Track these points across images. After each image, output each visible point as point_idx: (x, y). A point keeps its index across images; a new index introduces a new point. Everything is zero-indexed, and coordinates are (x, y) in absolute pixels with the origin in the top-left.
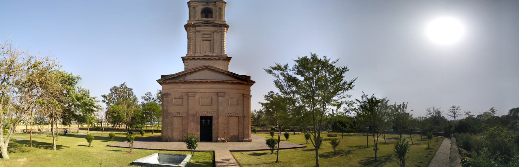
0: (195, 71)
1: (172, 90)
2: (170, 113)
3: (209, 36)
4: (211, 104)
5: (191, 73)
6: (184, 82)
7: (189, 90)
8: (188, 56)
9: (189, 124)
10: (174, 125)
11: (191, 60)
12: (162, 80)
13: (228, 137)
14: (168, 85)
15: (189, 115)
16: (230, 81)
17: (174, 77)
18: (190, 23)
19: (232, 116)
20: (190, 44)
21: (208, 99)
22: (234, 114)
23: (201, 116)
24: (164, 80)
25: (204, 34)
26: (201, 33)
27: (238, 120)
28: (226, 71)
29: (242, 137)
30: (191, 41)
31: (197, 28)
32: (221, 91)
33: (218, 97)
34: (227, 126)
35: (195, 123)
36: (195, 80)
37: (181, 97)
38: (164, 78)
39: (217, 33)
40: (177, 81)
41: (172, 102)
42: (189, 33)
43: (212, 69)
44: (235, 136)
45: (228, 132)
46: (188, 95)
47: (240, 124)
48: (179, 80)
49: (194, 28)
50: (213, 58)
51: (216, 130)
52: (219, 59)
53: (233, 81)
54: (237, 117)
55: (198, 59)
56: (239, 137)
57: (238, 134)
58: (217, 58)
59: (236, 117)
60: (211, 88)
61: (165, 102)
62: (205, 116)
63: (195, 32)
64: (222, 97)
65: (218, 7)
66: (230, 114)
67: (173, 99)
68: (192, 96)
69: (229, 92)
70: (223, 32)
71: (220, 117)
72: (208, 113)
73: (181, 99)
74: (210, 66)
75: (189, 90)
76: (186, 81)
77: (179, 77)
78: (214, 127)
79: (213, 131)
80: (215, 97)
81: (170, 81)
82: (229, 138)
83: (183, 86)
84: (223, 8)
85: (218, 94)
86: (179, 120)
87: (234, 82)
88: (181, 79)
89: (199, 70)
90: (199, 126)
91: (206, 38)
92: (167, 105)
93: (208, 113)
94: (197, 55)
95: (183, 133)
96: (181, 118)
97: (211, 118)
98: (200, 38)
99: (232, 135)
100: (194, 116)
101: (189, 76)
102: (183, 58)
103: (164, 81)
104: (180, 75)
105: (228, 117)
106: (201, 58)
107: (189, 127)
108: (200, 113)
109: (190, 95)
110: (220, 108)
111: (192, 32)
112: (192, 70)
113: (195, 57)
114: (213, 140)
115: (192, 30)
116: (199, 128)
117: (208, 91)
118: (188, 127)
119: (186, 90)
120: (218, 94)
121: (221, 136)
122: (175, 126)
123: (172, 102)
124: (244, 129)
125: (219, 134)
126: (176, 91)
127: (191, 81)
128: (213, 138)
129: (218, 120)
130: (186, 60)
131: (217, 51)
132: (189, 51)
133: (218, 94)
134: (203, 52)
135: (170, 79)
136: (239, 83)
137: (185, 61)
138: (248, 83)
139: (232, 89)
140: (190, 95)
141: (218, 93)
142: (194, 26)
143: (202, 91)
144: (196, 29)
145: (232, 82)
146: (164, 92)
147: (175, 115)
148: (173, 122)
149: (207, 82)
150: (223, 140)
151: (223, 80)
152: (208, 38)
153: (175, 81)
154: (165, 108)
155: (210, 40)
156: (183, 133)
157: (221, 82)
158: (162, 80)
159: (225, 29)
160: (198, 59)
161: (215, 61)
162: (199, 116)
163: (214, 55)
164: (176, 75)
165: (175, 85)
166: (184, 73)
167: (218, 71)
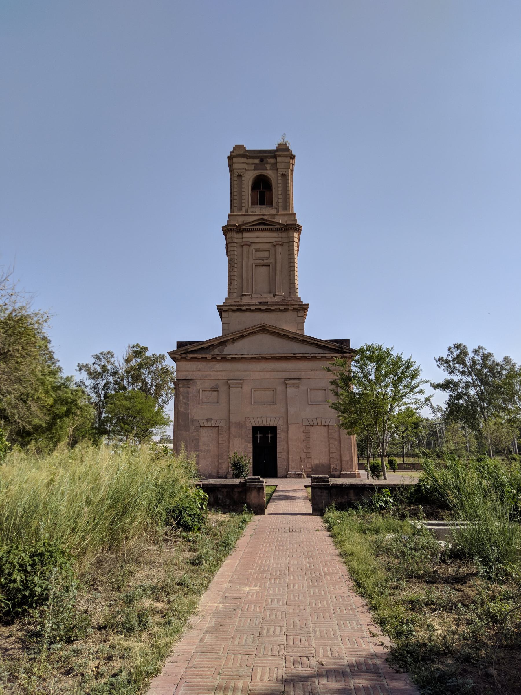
0: (243, 337)
1: (197, 373)
2: (193, 421)
3: (265, 255)
4: (274, 402)
5: (234, 340)
6: (222, 358)
7: (231, 375)
8: (231, 302)
9: (231, 442)
10: (201, 443)
11: (234, 311)
12: (179, 353)
13: (309, 468)
14: (191, 363)
15: (231, 424)
16: (309, 355)
17: (203, 348)
18: (232, 223)
19: (316, 424)
20: (232, 274)
21: (267, 392)
22: (319, 420)
23: (255, 425)
24: (184, 352)
25: (257, 250)
26: (254, 247)
27: (328, 431)
28: (299, 335)
29: (338, 468)
30: (234, 266)
31: (246, 235)
32: (293, 375)
33: (286, 388)
34: (305, 444)
35: (243, 440)
36: (242, 355)
37: (215, 389)
38: (182, 348)
39: (281, 247)
40: (209, 356)
41: (197, 397)
42: (232, 249)
43: (274, 332)
44: (323, 465)
45: (309, 458)
46: (229, 385)
47: (331, 441)
48: (212, 355)
49: (240, 235)
50: (276, 307)
51: (285, 454)
52: (286, 310)
53: (314, 355)
54: (325, 426)
55: (247, 309)
56: (332, 467)
57: (330, 461)
58: (282, 308)
59: (323, 427)
60: (273, 370)
61: (181, 397)
62: (261, 425)
63: (242, 246)
64: (293, 387)
65: (280, 172)
66: (310, 420)
67: (199, 392)
68: (237, 386)
69: (309, 377)
70: (291, 243)
71: (290, 426)
72: (269, 419)
73: (215, 393)
74: (270, 326)
75: (232, 374)
76: (225, 356)
77: (211, 348)
78: (279, 449)
79: (278, 456)
80: (280, 388)
81: (195, 356)
82: (310, 470)
83: (219, 366)
84: (290, 172)
85: (285, 383)
86: (212, 435)
87: (317, 355)
88: (216, 351)
89: (249, 334)
90: (250, 446)
91: (260, 261)
92: (186, 404)
93: (269, 419)
94: (245, 301)
95: (220, 461)
96: (215, 430)
97: (273, 430)
98: (252, 261)
99: (316, 464)
100: (240, 425)
101: (231, 345)
102: (219, 308)
103: (183, 356)
104: (213, 345)
105: (307, 427)
106: (253, 308)
107: (231, 448)
108: (251, 419)
109: (233, 385)
110: (292, 410)
111: (235, 245)
112: (237, 334)
113: (241, 306)
114: (279, 475)
115: (236, 240)
116: (251, 450)
117: (267, 375)
118: (229, 447)
119: (225, 373)
120: (287, 382)
121: (293, 465)
122: (202, 447)
123: (198, 398)
124: (340, 451)
125: (290, 463)
126: (206, 377)
127: (234, 356)
128: (278, 468)
129: (288, 433)
130: (225, 311)
131: (281, 293)
132: (231, 291)
133: (287, 382)
134: (256, 293)
135: (194, 350)
136: (326, 357)
137: (224, 314)
138: (345, 355)
139: (312, 371)
140: (233, 385)
141: (285, 380)
142: (240, 230)
143: (257, 376)
144: (243, 238)
145: (312, 357)
146: (182, 376)
147: (202, 425)
148: (198, 439)
149: (265, 358)
150: (299, 474)
151: (294, 354)
152: (265, 261)
153: (204, 356)
154: (182, 410)
155: (269, 266)
156: (220, 461)
157: (292, 357)
158: (179, 353)
159: (296, 235)
160: (248, 310)
161: (279, 314)
162: (250, 425)
163: (277, 299)
164: (207, 343)
165: (204, 363)
166: (220, 339)
167: (284, 335)
